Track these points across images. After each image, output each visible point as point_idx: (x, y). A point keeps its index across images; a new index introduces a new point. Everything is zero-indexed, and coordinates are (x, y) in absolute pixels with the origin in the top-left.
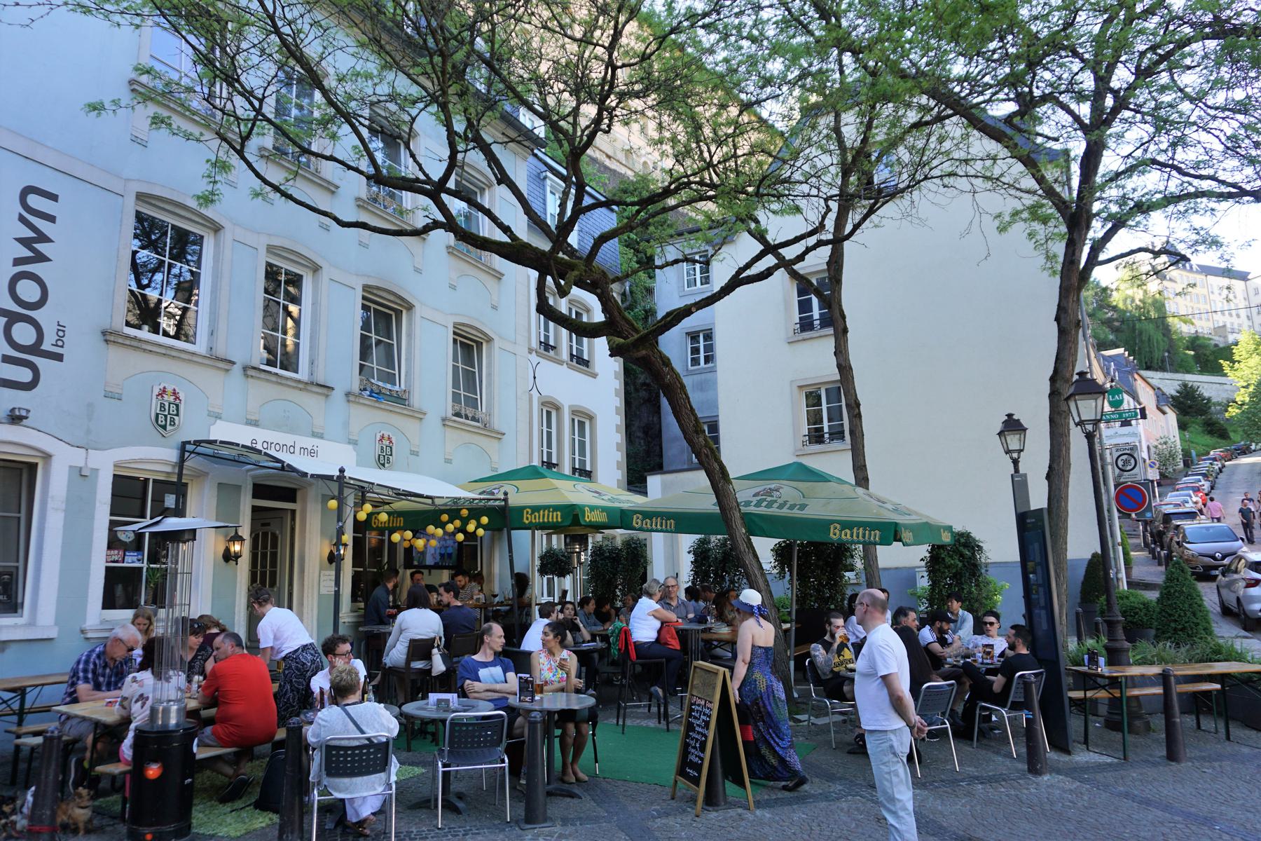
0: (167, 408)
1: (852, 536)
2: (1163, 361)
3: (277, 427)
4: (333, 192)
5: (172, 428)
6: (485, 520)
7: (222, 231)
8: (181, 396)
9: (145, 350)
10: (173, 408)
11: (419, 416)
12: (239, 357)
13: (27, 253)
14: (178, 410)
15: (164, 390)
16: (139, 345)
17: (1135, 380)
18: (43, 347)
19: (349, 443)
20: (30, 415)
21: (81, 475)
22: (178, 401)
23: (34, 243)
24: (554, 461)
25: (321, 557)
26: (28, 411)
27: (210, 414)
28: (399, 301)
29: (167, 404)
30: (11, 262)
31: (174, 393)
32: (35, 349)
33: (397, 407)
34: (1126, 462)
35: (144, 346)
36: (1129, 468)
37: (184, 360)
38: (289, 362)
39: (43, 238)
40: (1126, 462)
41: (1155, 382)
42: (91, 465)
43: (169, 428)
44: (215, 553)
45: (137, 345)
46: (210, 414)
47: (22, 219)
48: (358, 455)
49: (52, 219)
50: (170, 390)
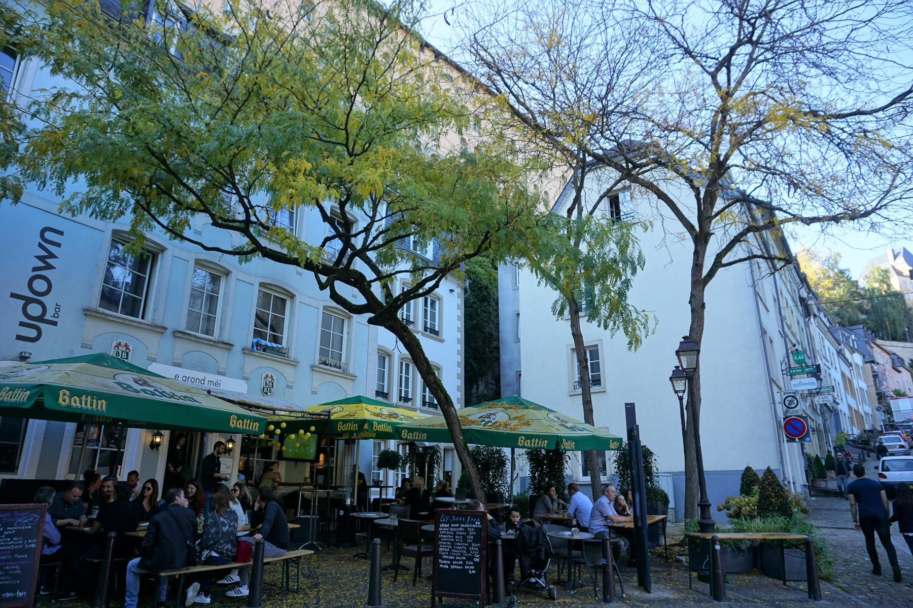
1: (81, 403)
2: (904, 335)
3: (194, 367)
6: (313, 428)
7: (166, 252)
8: (131, 348)
9: (109, 320)
11: (294, 364)
12: (171, 325)
13: (42, 265)
14: (127, 355)
16: (105, 317)
17: (872, 347)
18: (45, 318)
19: (243, 379)
20: (31, 356)
24: (410, 397)
25: (145, 443)
26: (30, 354)
29: (120, 352)
30: (31, 269)
32: (41, 319)
33: (279, 358)
34: (791, 402)
35: (109, 318)
36: (793, 406)
39: (52, 256)
40: (791, 402)
41: (889, 349)
45: (105, 318)
47: (40, 245)
49: (59, 245)
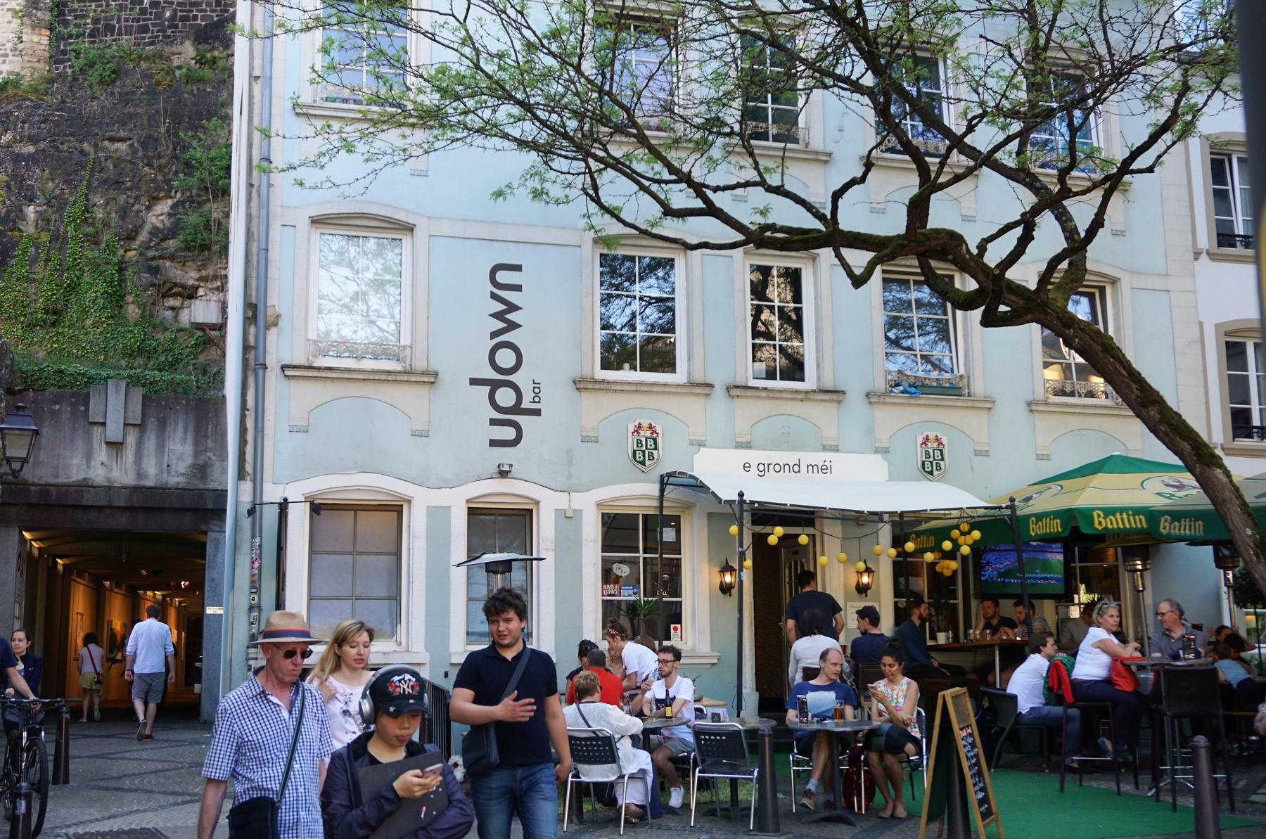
0: (644, 443)
4: (826, 162)
5: (651, 462)
8: (659, 429)
10: (937, 453)
11: (987, 405)
13: (502, 325)
14: (942, 455)
15: (640, 426)
16: (609, 386)
20: (513, 469)
21: (568, 518)
22: (941, 447)
23: (506, 317)
25: (846, 587)
26: (511, 466)
27: (692, 443)
28: (1100, 279)
31: (650, 427)
32: (517, 409)
35: (614, 387)
37: (657, 393)
38: (794, 369)
39: (513, 308)
42: (575, 506)
43: (647, 463)
44: (710, 584)
46: (692, 443)
47: (494, 296)
48: (890, 465)
49: (518, 288)
50: (932, 437)
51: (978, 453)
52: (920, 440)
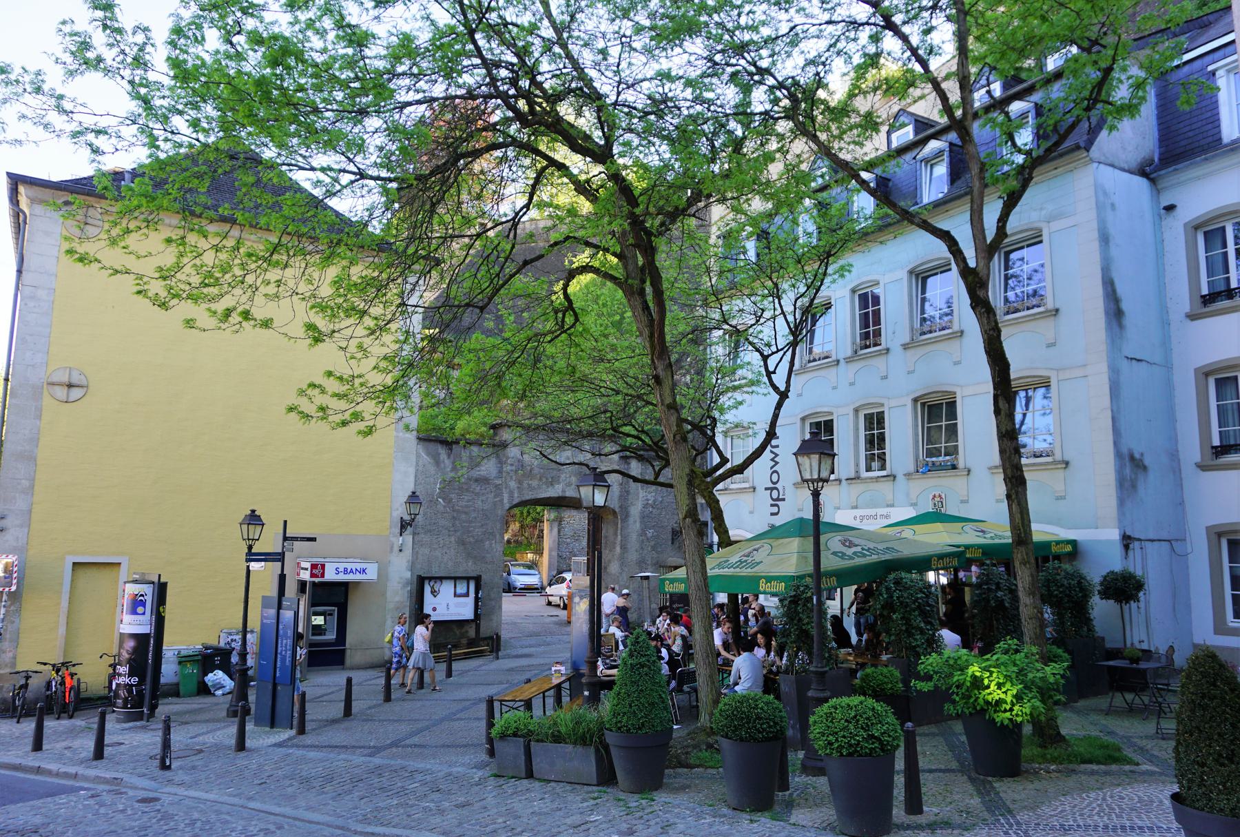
51: (962, 502)
52: (931, 497)
